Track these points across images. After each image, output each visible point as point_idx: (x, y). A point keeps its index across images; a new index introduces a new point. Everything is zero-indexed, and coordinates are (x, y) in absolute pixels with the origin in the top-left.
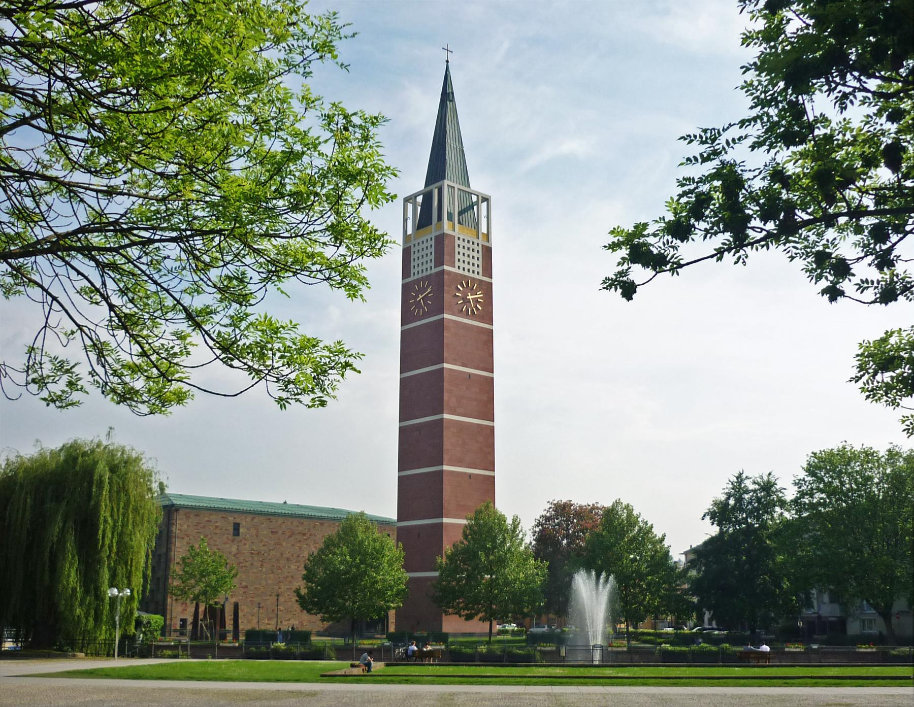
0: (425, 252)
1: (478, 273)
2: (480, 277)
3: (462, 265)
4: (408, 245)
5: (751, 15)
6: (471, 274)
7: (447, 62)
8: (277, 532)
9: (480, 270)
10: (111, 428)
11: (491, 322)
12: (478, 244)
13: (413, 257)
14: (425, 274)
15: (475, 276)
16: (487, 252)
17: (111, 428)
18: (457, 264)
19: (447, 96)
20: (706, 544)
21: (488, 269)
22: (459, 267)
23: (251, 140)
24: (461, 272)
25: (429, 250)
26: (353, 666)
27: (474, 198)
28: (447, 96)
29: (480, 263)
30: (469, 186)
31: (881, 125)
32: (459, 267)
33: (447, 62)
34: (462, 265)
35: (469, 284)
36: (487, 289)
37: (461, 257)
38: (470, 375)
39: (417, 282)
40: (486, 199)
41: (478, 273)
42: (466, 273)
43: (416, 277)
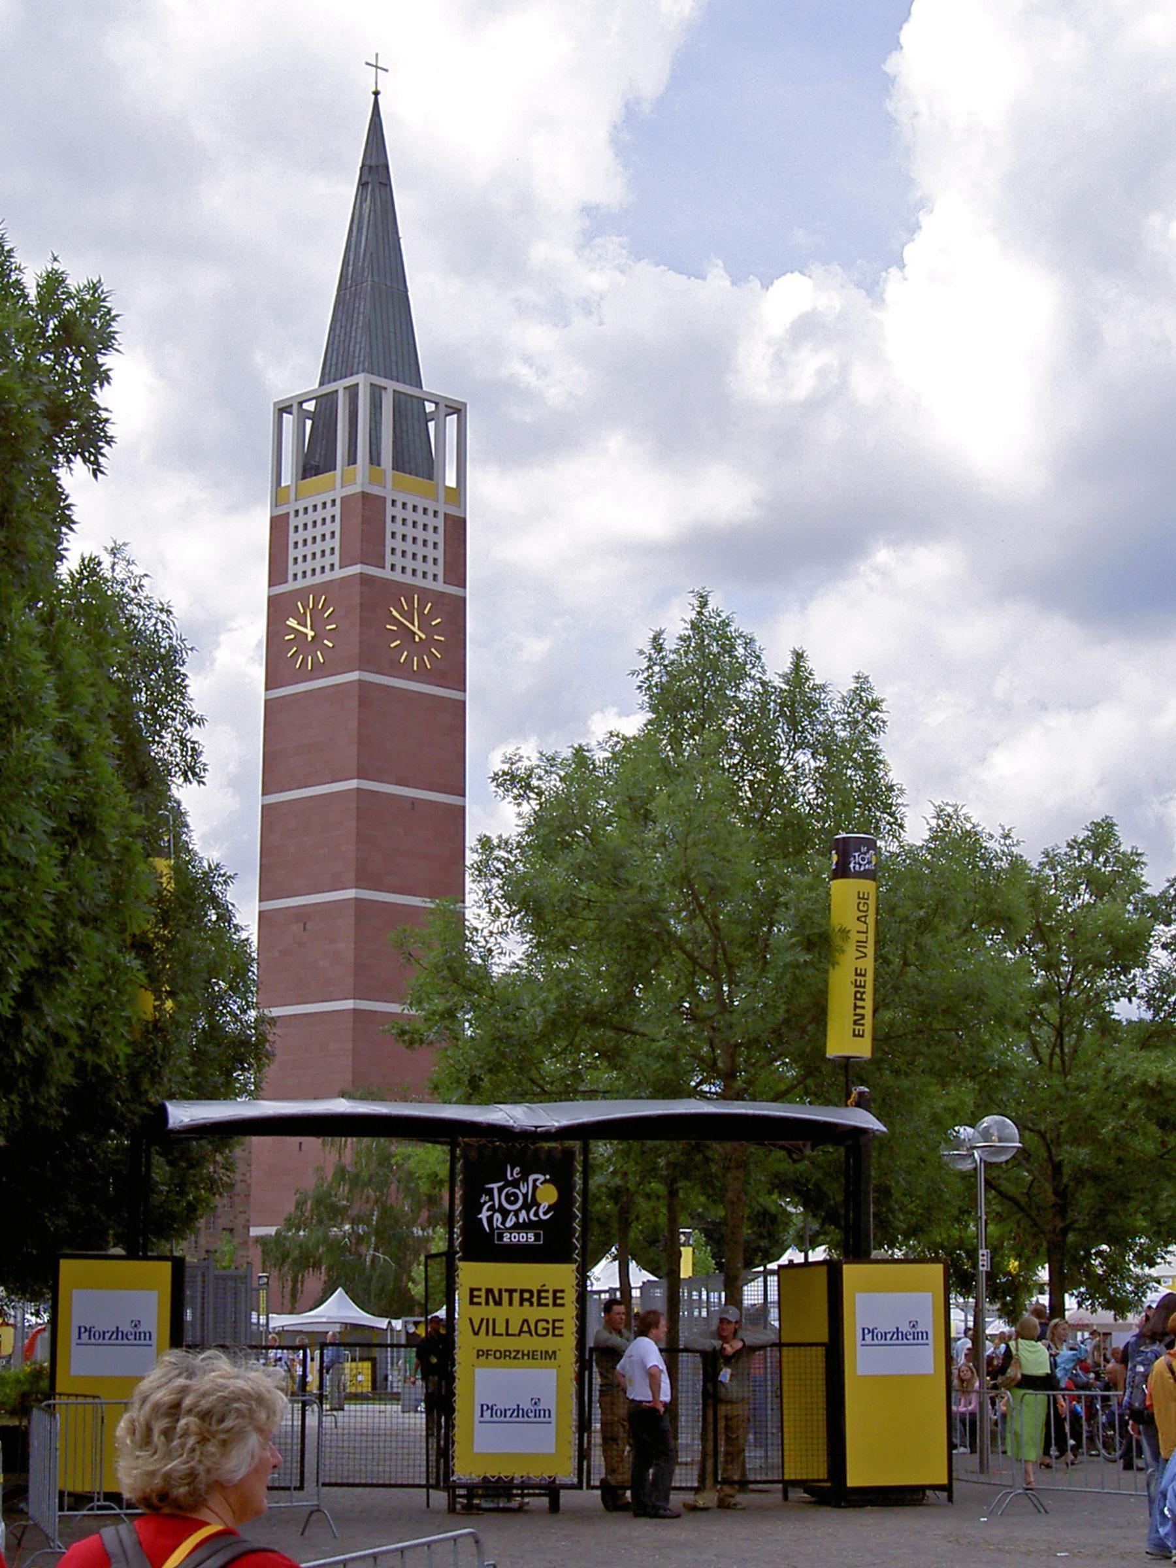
0: (309, 534)
2: (439, 586)
3: (399, 561)
4: (281, 511)
6: (419, 581)
7: (376, 93)
9: (440, 570)
10: (905, 279)
11: (460, 683)
13: (292, 537)
15: (429, 584)
16: (457, 529)
17: (905, 279)
19: (375, 176)
20: (454, 1341)
21: (456, 569)
22: (393, 567)
24: (397, 576)
25: (330, 511)
26: (312, 1359)
27: (430, 407)
28: (375, 176)
34: (399, 561)
37: (399, 544)
38: (414, 801)
39: (302, 594)
40: (458, 410)
42: (408, 579)
43: (301, 583)
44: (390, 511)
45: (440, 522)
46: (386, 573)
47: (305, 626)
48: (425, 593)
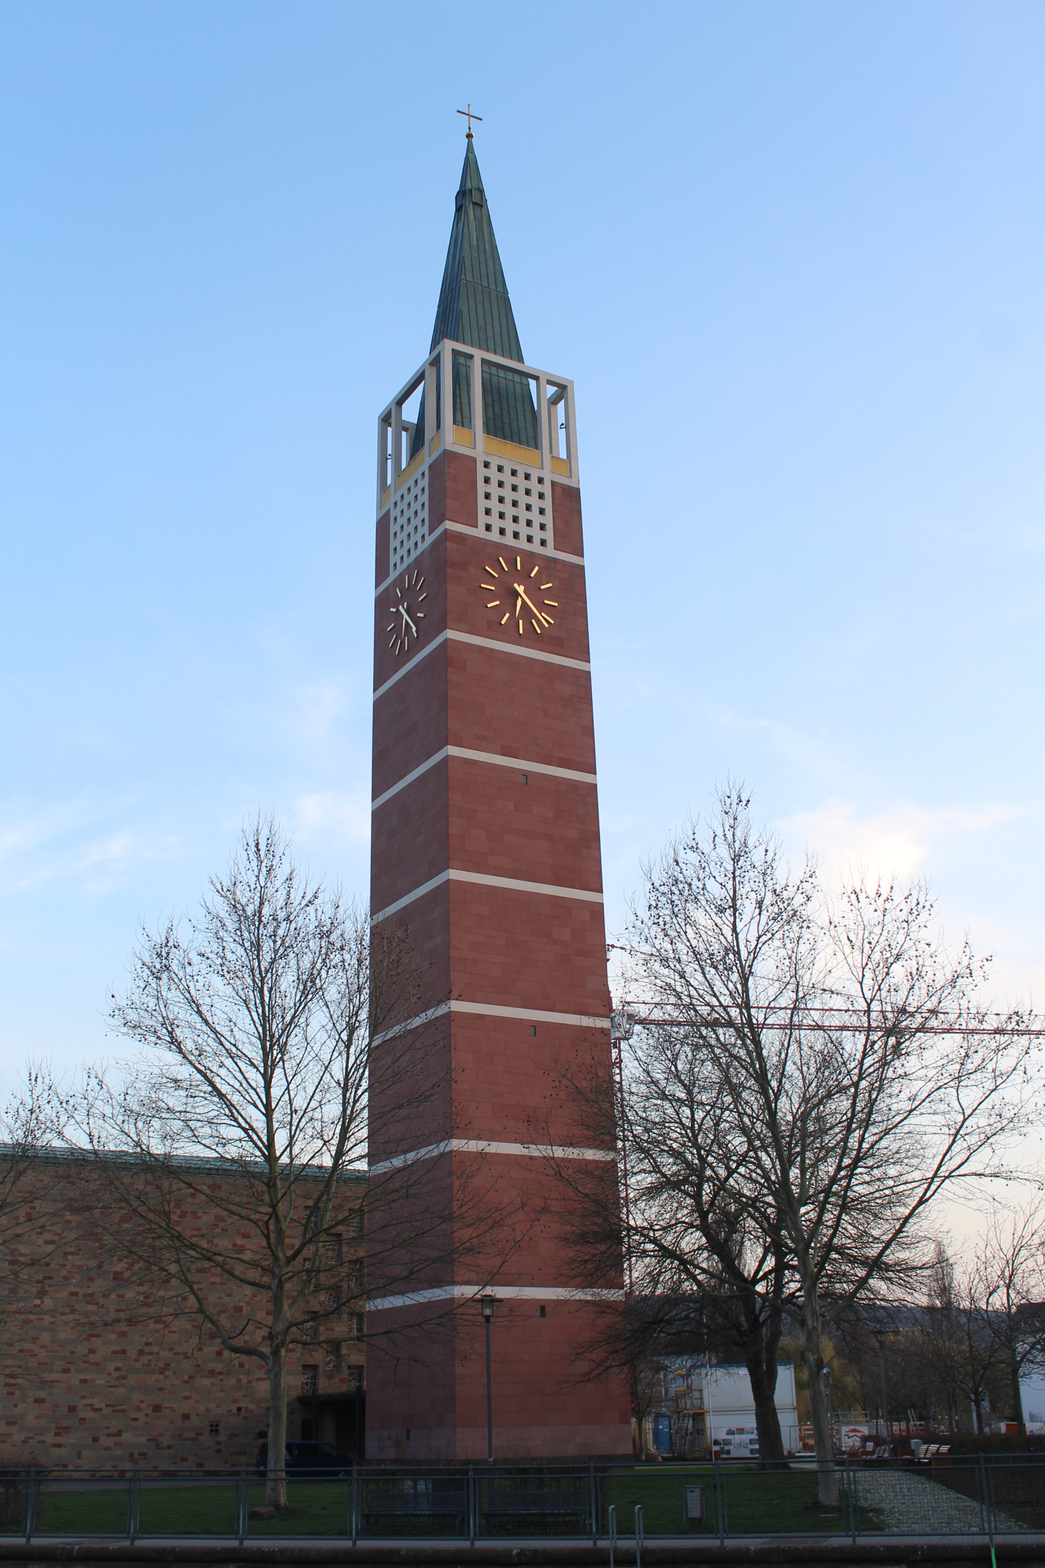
1: (543, 543)
2: (550, 551)
5: (744, 799)
6: (522, 544)
7: (469, 136)
8: (89, 1209)
9: (549, 535)
11: (583, 652)
12: (541, 481)
13: (393, 543)
14: (407, 561)
15: (535, 548)
18: (482, 519)
21: (569, 532)
22: (488, 528)
23: (699, 1115)
24: (494, 536)
28: (470, 199)
29: (548, 519)
30: (520, 359)
31: (147, 1415)
32: (488, 528)
33: (469, 136)
35: (523, 565)
36: (571, 586)
41: (543, 543)
42: (509, 540)
44: (481, 472)
45: (547, 489)
46: (480, 532)
47: (484, 361)
48: (530, 558)
